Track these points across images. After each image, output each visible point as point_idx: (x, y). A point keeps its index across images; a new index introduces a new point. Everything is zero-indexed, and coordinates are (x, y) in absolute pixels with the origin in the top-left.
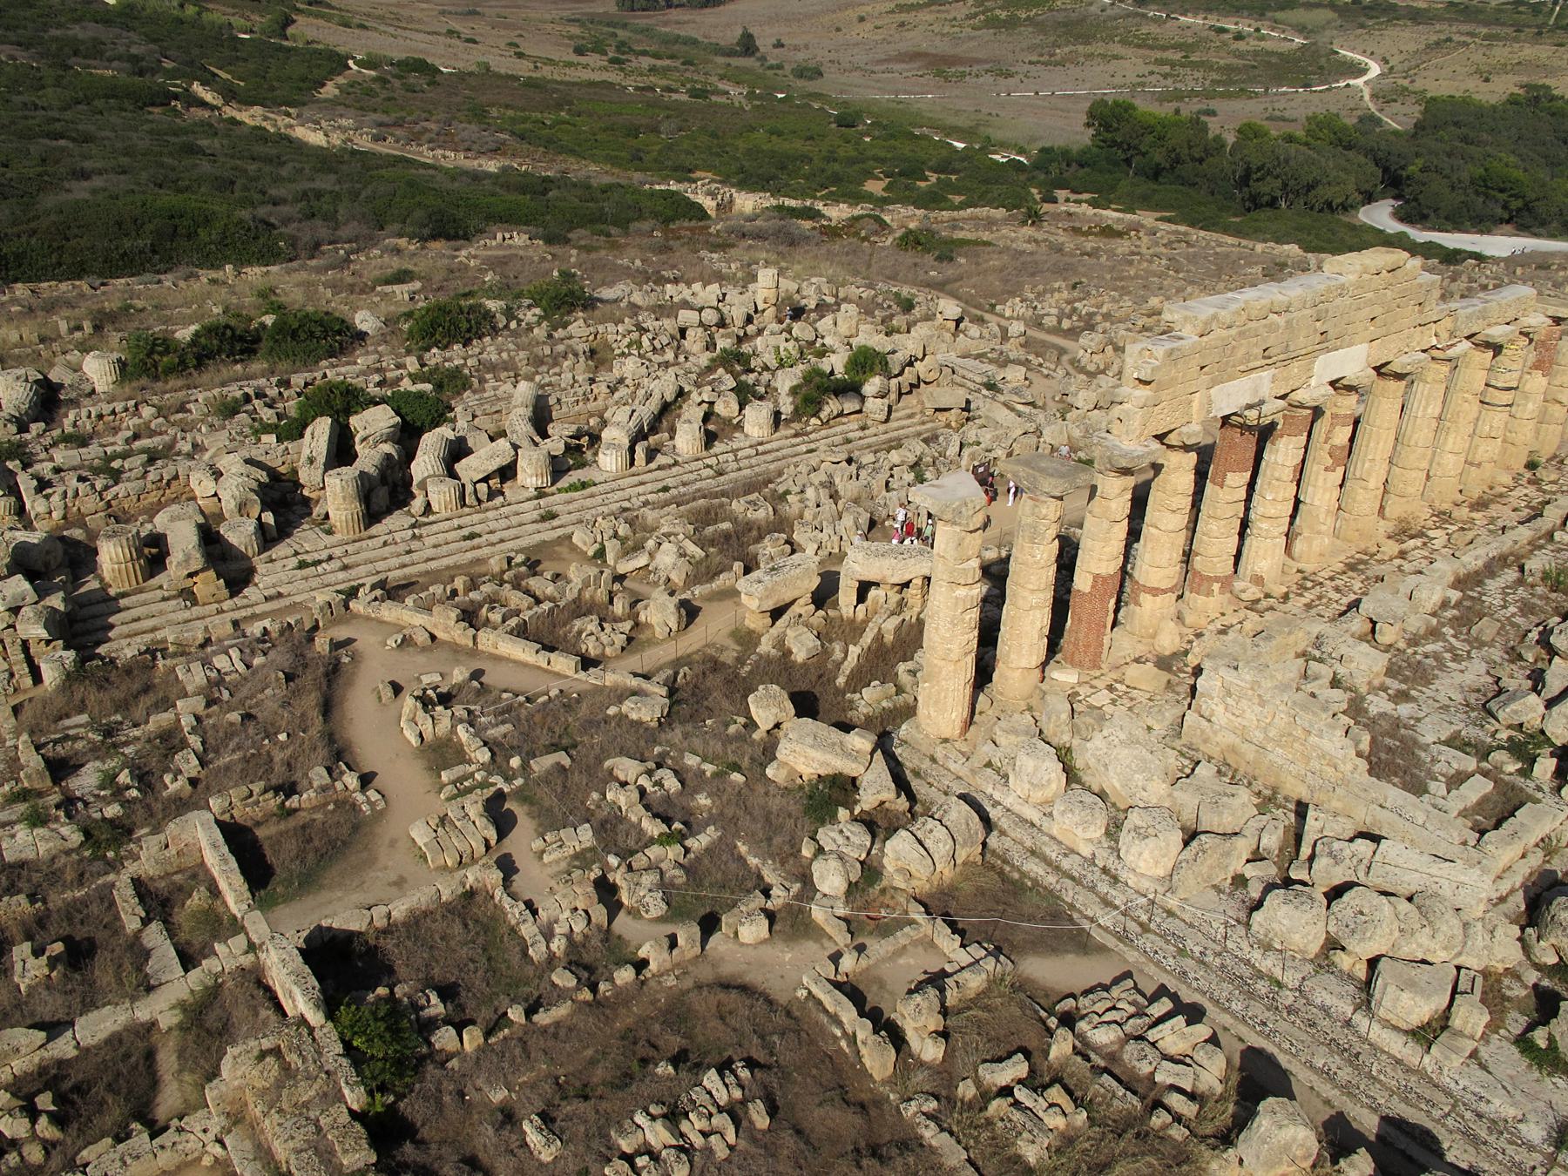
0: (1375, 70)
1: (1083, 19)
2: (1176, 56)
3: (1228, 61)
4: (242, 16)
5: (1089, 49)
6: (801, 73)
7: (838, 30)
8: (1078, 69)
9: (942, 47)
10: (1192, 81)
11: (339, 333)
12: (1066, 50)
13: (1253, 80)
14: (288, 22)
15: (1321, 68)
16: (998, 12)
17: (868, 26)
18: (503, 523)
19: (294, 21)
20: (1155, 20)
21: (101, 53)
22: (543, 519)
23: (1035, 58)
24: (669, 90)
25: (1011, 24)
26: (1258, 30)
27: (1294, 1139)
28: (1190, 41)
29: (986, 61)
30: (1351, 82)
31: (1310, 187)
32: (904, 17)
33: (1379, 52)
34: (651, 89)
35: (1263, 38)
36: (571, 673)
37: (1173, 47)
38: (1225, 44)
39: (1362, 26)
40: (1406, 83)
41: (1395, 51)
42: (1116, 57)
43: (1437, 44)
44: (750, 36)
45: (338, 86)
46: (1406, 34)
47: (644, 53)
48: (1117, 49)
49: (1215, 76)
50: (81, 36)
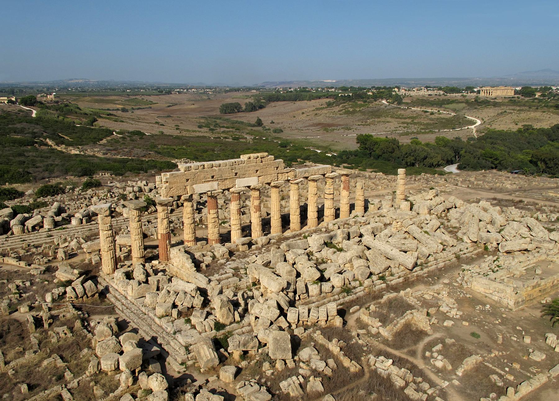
0: (479, 122)
1: (378, 110)
2: (409, 121)
3: (427, 122)
4: (79, 119)
5: (379, 120)
6: (275, 131)
7: (294, 117)
8: (374, 126)
9: (329, 121)
10: (414, 128)
11: (14, 194)
12: (371, 120)
13: (435, 128)
14: (95, 120)
15: (460, 123)
16: (350, 109)
17: (305, 115)
18: (35, 238)
19: (97, 120)
20: (403, 109)
21: (24, 132)
22: (48, 237)
23: (360, 123)
24: (226, 138)
25: (354, 112)
26: (439, 111)
27: (104, 330)
28: (415, 116)
29: (343, 125)
30: (469, 127)
31: (425, 158)
32: (317, 112)
33: (481, 116)
34: (219, 138)
35: (440, 114)
36: (24, 266)
37: (409, 118)
38: (427, 116)
39: (476, 108)
40: (489, 126)
41: (486, 116)
42: (388, 122)
43: (501, 113)
44: (260, 120)
45: (107, 140)
46: (491, 110)
47: (223, 127)
48: (389, 119)
49: (422, 127)
50: (19, 127)
